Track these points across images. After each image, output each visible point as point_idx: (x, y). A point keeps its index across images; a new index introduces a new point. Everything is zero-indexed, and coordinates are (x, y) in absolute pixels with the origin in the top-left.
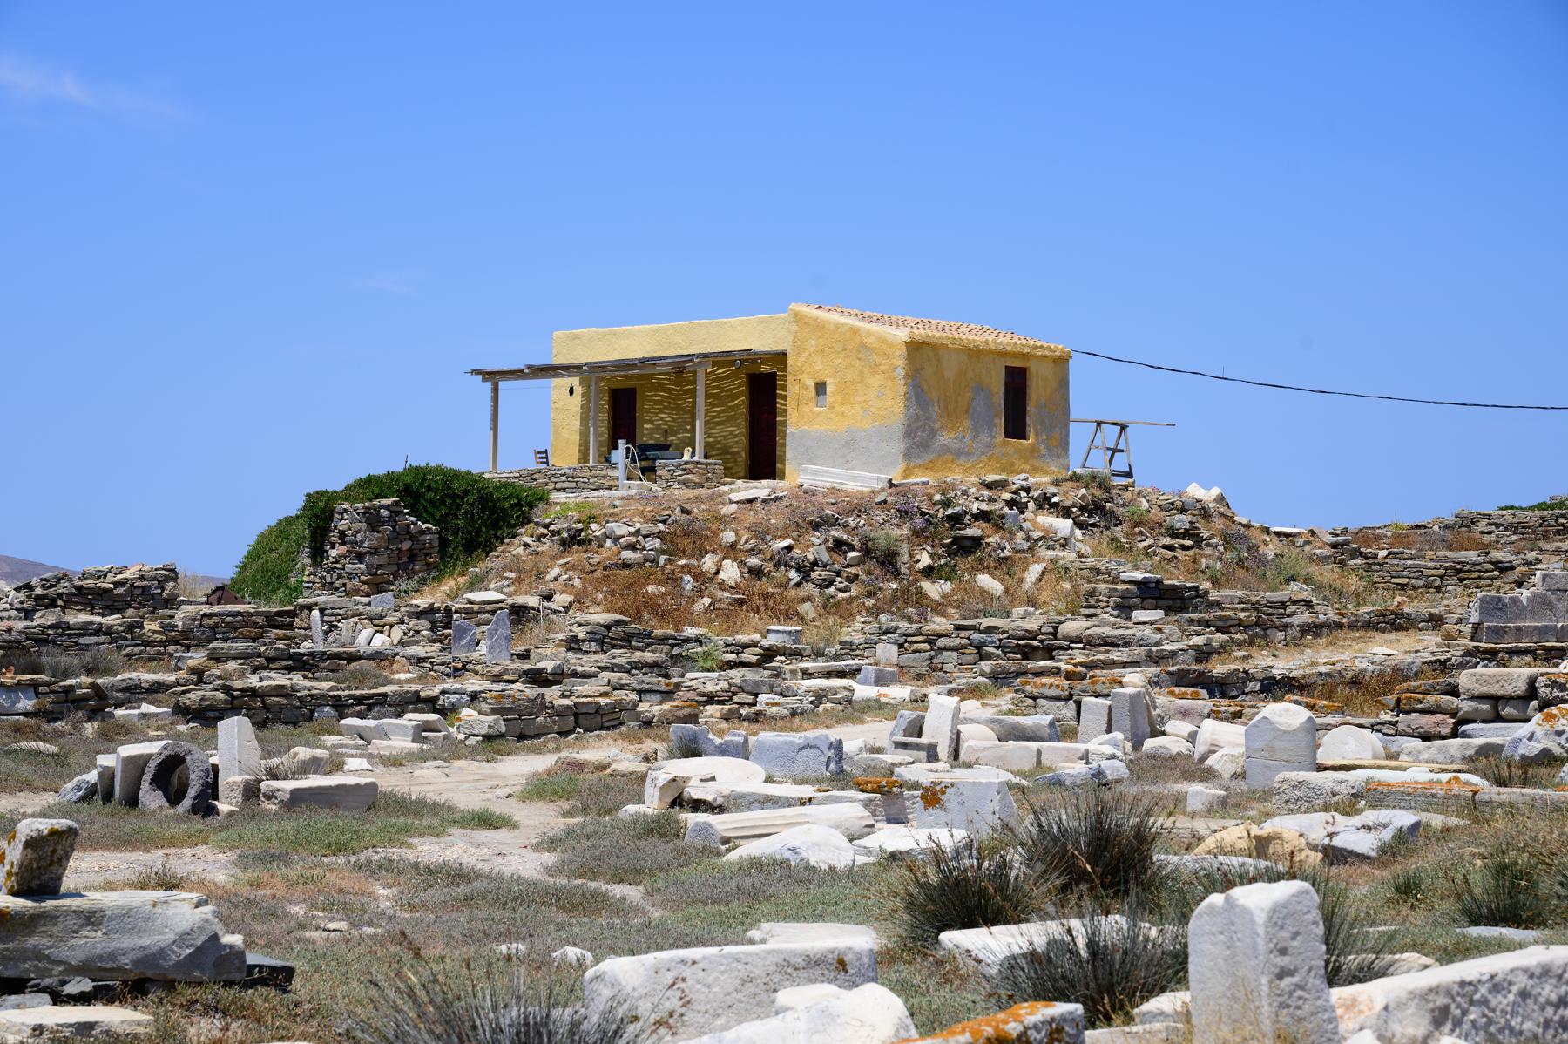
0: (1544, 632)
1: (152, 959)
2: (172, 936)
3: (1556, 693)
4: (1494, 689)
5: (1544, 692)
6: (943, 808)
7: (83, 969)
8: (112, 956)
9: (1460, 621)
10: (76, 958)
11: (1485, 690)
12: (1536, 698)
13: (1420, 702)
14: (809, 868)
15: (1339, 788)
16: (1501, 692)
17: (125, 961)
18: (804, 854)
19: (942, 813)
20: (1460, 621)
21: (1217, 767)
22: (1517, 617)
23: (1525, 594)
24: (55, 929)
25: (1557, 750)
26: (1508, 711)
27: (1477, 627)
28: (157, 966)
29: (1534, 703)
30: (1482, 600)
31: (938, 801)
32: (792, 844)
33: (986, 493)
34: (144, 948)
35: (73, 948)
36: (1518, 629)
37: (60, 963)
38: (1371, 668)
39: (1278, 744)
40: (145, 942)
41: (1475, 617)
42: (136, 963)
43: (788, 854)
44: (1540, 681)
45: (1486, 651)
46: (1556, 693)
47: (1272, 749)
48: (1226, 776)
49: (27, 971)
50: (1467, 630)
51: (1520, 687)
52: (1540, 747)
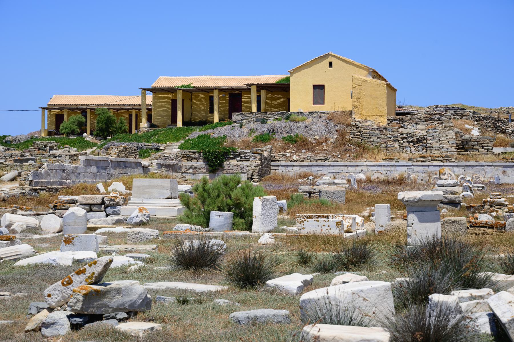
0: (48, 183)
1: (133, 304)
2: (137, 296)
3: (111, 203)
4: (91, 202)
5: (107, 202)
6: (73, 244)
7: (119, 309)
8: (123, 304)
9: (25, 180)
10: (115, 306)
11: (87, 202)
12: (104, 204)
13: (64, 206)
14: (60, 266)
15: (153, 234)
16: (93, 203)
17: (126, 305)
18: (58, 261)
19: (72, 246)
20: (25, 180)
21: (16, 229)
22: (41, 178)
23: (43, 171)
24: (110, 296)
25: (145, 221)
26: (95, 208)
27: (31, 182)
28: (133, 307)
29: (103, 206)
30: (33, 173)
31: (71, 242)
32: (53, 258)
33: (422, 159)
34: (131, 301)
35: (114, 302)
36: (42, 182)
37: (111, 308)
38: (7, 195)
39: (77, 221)
40: (131, 298)
41: (31, 178)
42: (129, 306)
43: (51, 262)
44: (105, 199)
45: (35, 190)
46: (111, 203)
47: (75, 222)
48: (19, 232)
49: (103, 311)
50: (28, 182)
51: (100, 201)
52: (140, 219)
